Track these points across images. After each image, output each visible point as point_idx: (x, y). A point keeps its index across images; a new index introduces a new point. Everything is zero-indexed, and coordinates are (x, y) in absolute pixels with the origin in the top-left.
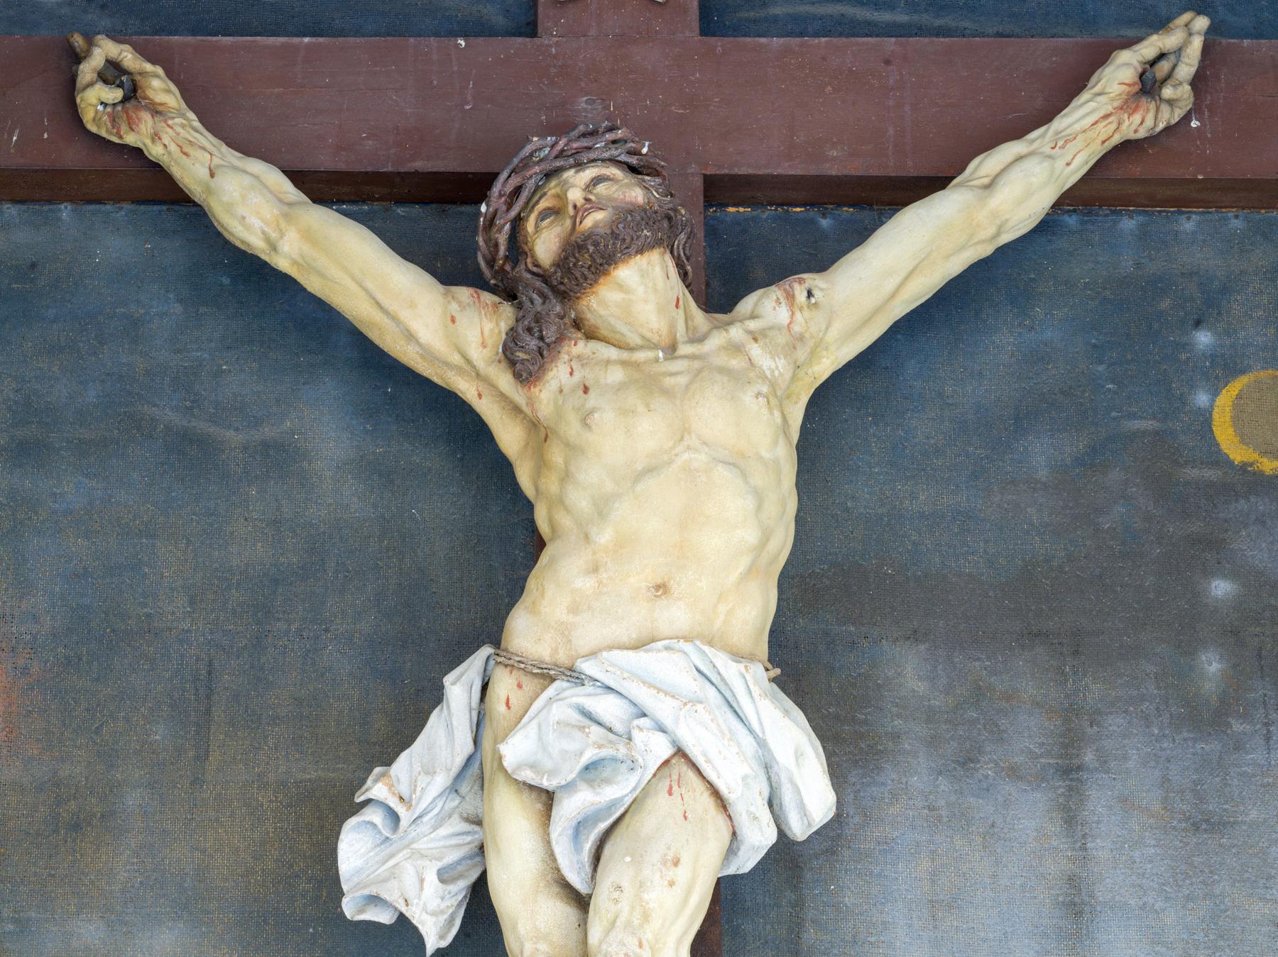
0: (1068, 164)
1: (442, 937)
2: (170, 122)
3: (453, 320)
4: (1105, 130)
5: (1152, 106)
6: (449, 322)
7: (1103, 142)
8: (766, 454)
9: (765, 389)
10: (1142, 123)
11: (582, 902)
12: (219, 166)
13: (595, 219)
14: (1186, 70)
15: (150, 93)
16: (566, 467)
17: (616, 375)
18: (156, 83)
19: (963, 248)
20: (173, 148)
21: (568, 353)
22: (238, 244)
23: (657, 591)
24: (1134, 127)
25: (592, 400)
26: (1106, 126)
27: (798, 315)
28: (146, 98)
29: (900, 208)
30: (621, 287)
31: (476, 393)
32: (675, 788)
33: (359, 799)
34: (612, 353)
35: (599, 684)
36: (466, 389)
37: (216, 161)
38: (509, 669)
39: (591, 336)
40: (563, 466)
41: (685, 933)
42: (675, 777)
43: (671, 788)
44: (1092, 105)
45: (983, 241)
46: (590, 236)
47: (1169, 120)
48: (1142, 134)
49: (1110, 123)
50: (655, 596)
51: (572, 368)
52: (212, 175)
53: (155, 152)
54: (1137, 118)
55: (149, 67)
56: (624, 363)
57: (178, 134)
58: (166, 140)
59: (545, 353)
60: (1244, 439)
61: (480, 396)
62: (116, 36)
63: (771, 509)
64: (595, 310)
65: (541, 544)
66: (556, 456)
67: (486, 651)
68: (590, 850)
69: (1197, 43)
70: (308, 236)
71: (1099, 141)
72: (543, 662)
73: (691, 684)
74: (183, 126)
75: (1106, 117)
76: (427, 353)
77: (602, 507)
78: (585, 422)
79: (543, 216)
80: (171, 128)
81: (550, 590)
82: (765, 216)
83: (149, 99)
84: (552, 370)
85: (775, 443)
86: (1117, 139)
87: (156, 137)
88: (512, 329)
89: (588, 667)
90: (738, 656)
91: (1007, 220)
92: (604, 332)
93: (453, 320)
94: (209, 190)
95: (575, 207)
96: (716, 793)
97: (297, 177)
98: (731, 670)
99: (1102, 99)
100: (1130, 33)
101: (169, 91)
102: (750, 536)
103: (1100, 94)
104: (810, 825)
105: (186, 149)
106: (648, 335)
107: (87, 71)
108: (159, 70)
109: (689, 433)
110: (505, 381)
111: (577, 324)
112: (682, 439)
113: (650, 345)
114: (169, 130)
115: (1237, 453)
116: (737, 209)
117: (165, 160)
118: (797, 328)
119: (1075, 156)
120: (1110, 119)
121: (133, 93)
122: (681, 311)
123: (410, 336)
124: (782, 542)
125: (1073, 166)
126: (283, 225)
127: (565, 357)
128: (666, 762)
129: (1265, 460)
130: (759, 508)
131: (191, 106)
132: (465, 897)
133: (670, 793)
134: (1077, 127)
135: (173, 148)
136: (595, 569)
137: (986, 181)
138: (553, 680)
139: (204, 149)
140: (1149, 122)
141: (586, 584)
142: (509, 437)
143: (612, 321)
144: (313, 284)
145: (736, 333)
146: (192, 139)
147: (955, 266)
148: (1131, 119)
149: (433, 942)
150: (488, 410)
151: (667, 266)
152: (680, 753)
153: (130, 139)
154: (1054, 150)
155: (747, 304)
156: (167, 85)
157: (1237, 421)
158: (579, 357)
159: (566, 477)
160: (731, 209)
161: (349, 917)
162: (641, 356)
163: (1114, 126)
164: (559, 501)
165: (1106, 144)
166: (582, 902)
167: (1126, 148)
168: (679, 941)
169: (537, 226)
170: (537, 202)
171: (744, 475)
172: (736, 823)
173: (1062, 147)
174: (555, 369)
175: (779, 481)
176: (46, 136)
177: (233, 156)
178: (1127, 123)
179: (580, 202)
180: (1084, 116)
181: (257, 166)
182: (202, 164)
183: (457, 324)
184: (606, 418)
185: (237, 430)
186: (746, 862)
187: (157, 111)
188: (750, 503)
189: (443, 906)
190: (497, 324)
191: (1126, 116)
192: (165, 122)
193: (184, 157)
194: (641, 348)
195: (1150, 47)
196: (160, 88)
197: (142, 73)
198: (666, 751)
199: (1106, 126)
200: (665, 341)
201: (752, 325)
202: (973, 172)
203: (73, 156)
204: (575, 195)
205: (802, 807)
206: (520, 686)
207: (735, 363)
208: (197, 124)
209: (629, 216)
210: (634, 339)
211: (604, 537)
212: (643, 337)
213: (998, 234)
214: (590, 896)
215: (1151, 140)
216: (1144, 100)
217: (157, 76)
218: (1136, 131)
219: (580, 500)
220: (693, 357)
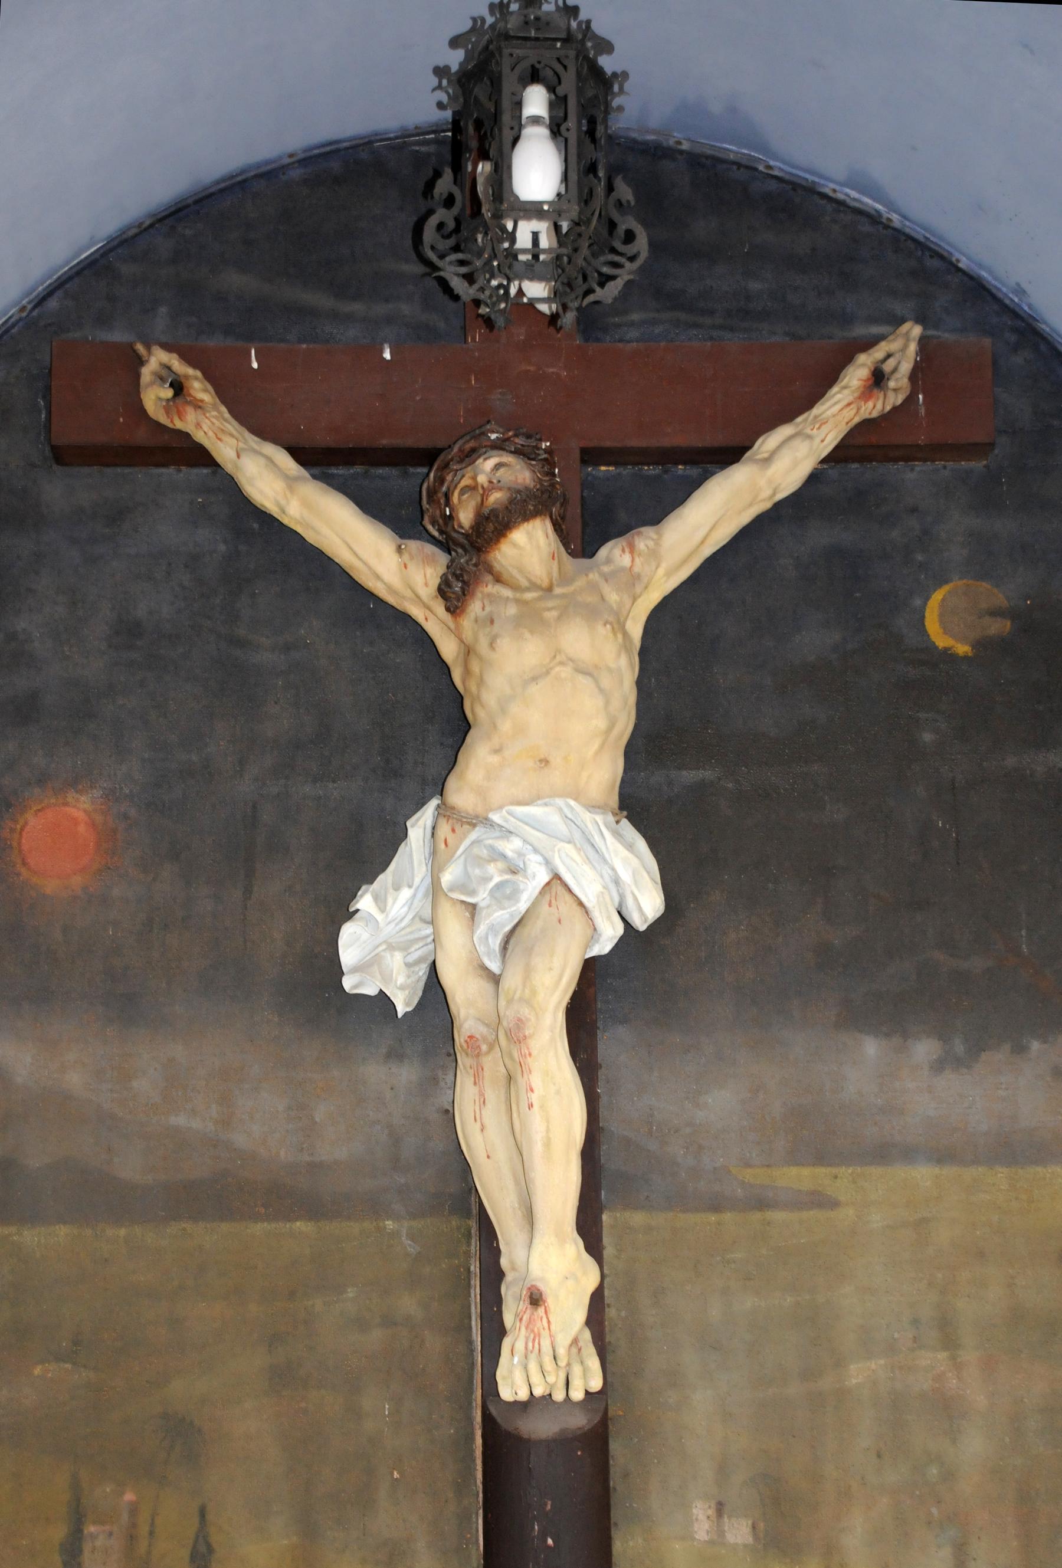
0: (822, 441)
1: (407, 1004)
2: (208, 415)
3: (406, 567)
4: (849, 413)
5: (881, 395)
6: (403, 568)
7: (847, 423)
8: (612, 665)
9: (611, 619)
10: (874, 408)
11: (495, 980)
12: (243, 449)
13: (496, 497)
14: (906, 367)
15: (192, 392)
16: (481, 674)
17: (512, 610)
18: (196, 385)
19: (750, 505)
20: (211, 434)
21: (482, 593)
22: (259, 506)
23: (541, 764)
24: (868, 411)
25: (496, 628)
26: (849, 411)
27: (637, 560)
28: (190, 395)
29: (717, 470)
30: (515, 545)
31: (424, 618)
32: (553, 901)
33: (352, 910)
34: (507, 592)
35: (504, 829)
36: (417, 613)
37: (241, 445)
38: (446, 818)
39: (498, 579)
40: (479, 675)
41: (560, 1002)
42: (553, 894)
43: (550, 901)
44: (839, 396)
45: (764, 500)
46: (494, 512)
47: (894, 403)
48: (875, 414)
49: (851, 409)
50: (540, 767)
51: (484, 604)
52: (238, 457)
53: (199, 437)
54: (870, 404)
55: (190, 371)
56: (517, 601)
57: (213, 423)
58: (205, 428)
59: (466, 592)
60: (946, 631)
61: (426, 619)
62: (167, 347)
63: (616, 703)
64: (499, 561)
65: (469, 727)
66: (475, 667)
67: (434, 802)
68: (500, 944)
69: (913, 347)
70: (305, 503)
71: (844, 423)
72: (468, 814)
73: (562, 828)
74: (215, 417)
75: (849, 404)
76: (390, 588)
77: (503, 710)
78: (492, 645)
79: (463, 492)
80: (209, 419)
81: (473, 764)
82: (624, 473)
83: (192, 396)
84: (471, 605)
85: (619, 655)
86: (857, 420)
87: (198, 425)
88: (444, 574)
89: (495, 817)
90: (593, 807)
91: (780, 484)
92: (505, 576)
93: (406, 567)
94: (236, 466)
95: (483, 487)
96: (581, 904)
97: (300, 454)
98: (587, 818)
99: (846, 392)
100: (875, 330)
101: (206, 390)
102: (600, 723)
103: (845, 387)
104: (646, 921)
105: (220, 435)
106: (533, 579)
107: (147, 373)
108: (199, 374)
109: (560, 652)
110: (439, 608)
111: (490, 570)
112: (555, 657)
113: (534, 586)
114: (207, 420)
115: (941, 641)
116: (607, 468)
117: (207, 444)
118: (636, 569)
119: (827, 434)
120: (852, 406)
121: (178, 387)
122: (556, 561)
123: (378, 577)
124: (625, 723)
125: (825, 442)
126: (289, 495)
127: (479, 595)
128: (548, 884)
129: (959, 645)
130: (607, 703)
131: (224, 402)
132: (425, 972)
133: (550, 905)
134: (829, 413)
135: (211, 434)
136: (497, 751)
137: (766, 455)
138: (474, 826)
139: (232, 435)
140: (879, 406)
141: (494, 759)
142: (448, 649)
143: (510, 569)
144: (310, 537)
145: (593, 576)
146: (224, 428)
147: (746, 518)
148: (866, 406)
149: (401, 1009)
150: (433, 628)
151: (546, 529)
152: (557, 877)
153: (179, 425)
154: (813, 431)
155: (603, 552)
156: (205, 386)
157: (941, 616)
158: (489, 595)
159: (481, 682)
160: (603, 468)
161: (347, 991)
162: (529, 596)
163: (854, 411)
164: (477, 699)
165: (849, 424)
166: (495, 980)
167: (866, 425)
168: (557, 1008)
169: (459, 499)
170: (459, 482)
171: (596, 681)
172: (595, 923)
173: (819, 428)
174: (473, 605)
175: (621, 682)
176: (121, 420)
177: (253, 440)
178: (863, 408)
179: (486, 485)
180: (830, 407)
181: (271, 450)
182: (231, 448)
183: (408, 569)
184: (505, 644)
185: (267, 637)
186: (604, 947)
187: (198, 405)
188: (600, 702)
189: (409, 981)
190: (435, 570)
191: (863, 403)
192: (204, 414)
193: (219, 442)
194: (528, 589)
195: (878, 353)
196: (199, 389)
197: (187, 377)
198: (544, 877)
199: (849, 411)
200: (545, 583)
201: (606, 569)
202: (759, 448)
203: (141, 436)
204: (482, 479)
205: (640, 909)
206: (453, 830)
207: (590, 599)
208: (227, 415)
209: (518, 495)
210: (524, 583)
211: (506, 726)
212: (530, 581)
213: (774, 494)
214: (500, 975)
215: (884, 417)
216: (875, 391)
217: (196, 378)
218: (870, 414)
219: (490, 699)
220: (563, 596)
